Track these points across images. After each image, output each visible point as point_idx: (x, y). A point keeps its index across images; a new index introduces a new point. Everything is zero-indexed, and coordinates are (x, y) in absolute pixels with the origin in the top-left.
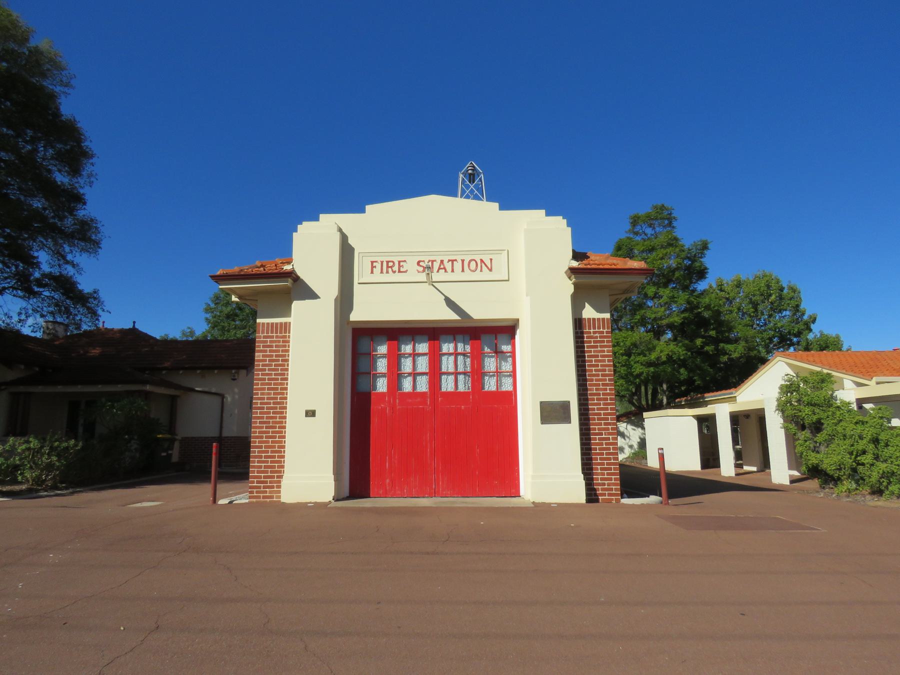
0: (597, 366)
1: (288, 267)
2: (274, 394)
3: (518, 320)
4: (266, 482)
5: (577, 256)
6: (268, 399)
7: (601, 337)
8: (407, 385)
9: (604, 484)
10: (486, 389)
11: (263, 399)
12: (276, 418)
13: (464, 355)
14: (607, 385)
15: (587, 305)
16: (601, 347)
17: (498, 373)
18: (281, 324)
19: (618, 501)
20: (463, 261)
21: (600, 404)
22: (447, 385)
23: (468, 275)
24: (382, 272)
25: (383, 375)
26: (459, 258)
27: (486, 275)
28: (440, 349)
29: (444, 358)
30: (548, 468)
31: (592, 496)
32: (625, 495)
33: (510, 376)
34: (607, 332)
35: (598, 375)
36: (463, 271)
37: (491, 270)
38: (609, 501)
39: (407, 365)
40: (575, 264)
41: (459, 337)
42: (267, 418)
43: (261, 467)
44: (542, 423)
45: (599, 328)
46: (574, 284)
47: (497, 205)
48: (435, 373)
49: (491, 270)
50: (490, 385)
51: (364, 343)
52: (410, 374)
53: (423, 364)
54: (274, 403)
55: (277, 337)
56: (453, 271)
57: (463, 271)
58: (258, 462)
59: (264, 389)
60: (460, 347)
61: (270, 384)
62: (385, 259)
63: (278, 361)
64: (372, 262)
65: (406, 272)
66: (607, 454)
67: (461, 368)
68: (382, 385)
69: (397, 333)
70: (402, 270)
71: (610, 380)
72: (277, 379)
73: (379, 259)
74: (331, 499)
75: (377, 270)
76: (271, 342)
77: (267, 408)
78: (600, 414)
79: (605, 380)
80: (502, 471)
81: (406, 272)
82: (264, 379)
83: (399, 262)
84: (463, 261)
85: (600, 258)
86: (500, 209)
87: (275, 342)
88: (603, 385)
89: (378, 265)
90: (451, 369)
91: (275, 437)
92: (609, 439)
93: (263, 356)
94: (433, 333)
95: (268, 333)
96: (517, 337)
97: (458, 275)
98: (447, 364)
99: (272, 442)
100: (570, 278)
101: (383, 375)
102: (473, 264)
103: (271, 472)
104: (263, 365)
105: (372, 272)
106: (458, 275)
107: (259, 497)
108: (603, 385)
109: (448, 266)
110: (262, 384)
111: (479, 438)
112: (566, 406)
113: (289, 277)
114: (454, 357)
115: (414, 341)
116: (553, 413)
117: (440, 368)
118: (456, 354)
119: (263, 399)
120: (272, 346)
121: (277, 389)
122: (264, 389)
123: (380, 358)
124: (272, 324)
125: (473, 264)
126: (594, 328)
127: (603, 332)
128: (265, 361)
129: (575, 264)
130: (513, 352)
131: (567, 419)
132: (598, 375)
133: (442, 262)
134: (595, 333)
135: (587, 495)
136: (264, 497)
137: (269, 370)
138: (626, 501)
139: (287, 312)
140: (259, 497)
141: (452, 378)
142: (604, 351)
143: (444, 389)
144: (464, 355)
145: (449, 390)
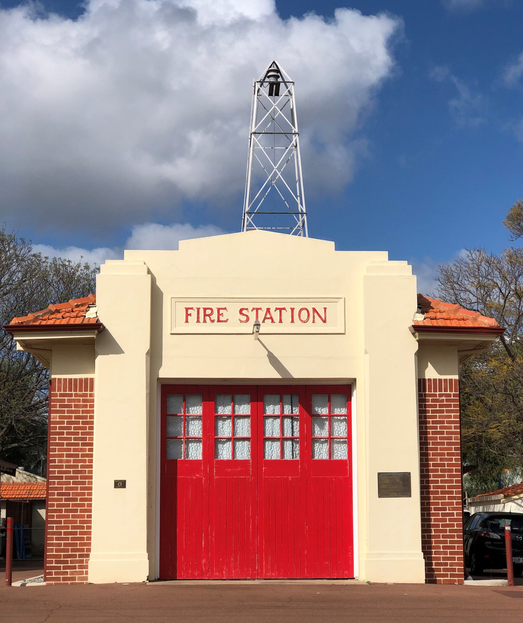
0: (443, 433)
1: (91, 314)
2: (74, 461)
3: (355, 380)
4: (67, 562)
5: (423, 305)
6: (67, 467)
7: (447, 401)
8: (225, 453)
9: (446, 564)
10: (316, 458)
11: (62, 467)
12: (77, 489)
13: (292, 417)
14: (453, 455)
15: (38, 510)
16: (447, 411)
17: (330, 440)
18: (81, 380)
19: (461, 583)
20: (292, 310)
21: (444, 476)
22: (272, 452)
23: (298, 327)
24: (198, 321)
25: (196, 440)
26: (288, 307)
27: (319, 327)
28: (264, 411)
29: (269, 422)
30: (386, 544)
31: (431, 576)
32: (470, 577)
33: (344, 442)
34: (455, 395)
35: (443, 444)
36: (292, 321)
37: (325, 321)
38: (451, 583)
39: (225, 429)
40: (420, 318)
41: (287, 398)
42: (66, 489)
43: (60, 545)
44: (380, 496)
45: (446, 390)
46: (418, 341)
47: (332, 244)
48: (258, 439)
49: (325, 321)
50: (321, 452)
51: (175, 403)
52: (229, 439)
53: (244, 428)
54: (74, 472)
55: (76, 395)
56: (281, 321)
57: (292, 321)
58: (57, 539)
59: (62, 456)
60: (287, 410)
61: (69, 450)
62: (202, 306)
63: (78, 423)
64: (187, 309)
65: (226, 321)
66: (450, 531)
67: (288, 434)
68: (196, 452)
69: (212, 392)
70: (221, 318)
71: (456, 449)
72: (78, 444)
73: (195, 306)
74: (145, 579)
75: (193, 318)
76: (69, 401)
77: (67, 478)
78: (444, 487)
79: (451, 449)
80: (334, 546)
81: (226, 321)
82: (62, 444)
83: (219, 309)
84: (292, 310)
85: (448, 314)
86: (337, 249)
87: (74, 401)
88: (448, 454)
89: (194, 313)
90: (277, 434)
91: (76, 511)
92: (453, 514)
93: (60, 417)
94: (256, 392)
95: (65, 390)
96: (354, 399)
97: (286, 327)
98: (272, 428)
99: (73, 516)
100: (413, 334)
101: (196, 440)
102: (304, 314)
103: (72, 550)
104: (60, 428)
105: (187, 321)
106: (286, 327)
107: (59, 579)
108: (448, 454)
109: (276, 315)
110: (60, 450)
111: (311, 509)
112: (406, 477)
113: (95, 329)
114: (280, 421)
115: (234, 402)
116: (392, 485)
117: (264, 433)
118: (282, 417)
119: (62, 467)
120: (70, 406)
121: (77, 455)
122: (62, 456)
123: (193, 419)
124: (70, 380)
125: (304, 314)
126: (440, 390)
127: (449, 395)
128: (63, 423)
129: (420, 318)
130: (349, 415)
131: (406, 492)
132: (443, 444)
133: (268, 310)
134: (441, 395)
135: (427, 576)
136: (64, 579)
137: (68, 433)
138: (470, 582)
139: (92, 368)
140: (59, 579)
141: (277, 444)
142: (450, 417)
143: (268, 457)
144: (292, 417)
145: (274, 458)
